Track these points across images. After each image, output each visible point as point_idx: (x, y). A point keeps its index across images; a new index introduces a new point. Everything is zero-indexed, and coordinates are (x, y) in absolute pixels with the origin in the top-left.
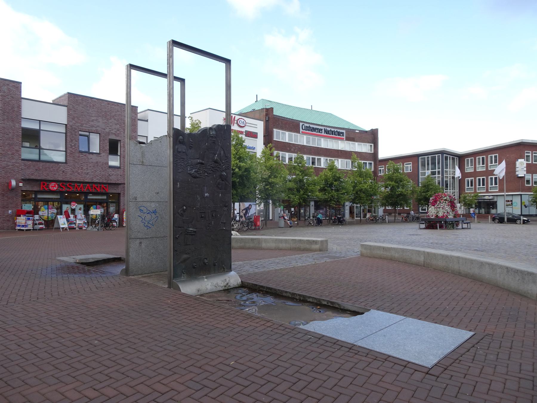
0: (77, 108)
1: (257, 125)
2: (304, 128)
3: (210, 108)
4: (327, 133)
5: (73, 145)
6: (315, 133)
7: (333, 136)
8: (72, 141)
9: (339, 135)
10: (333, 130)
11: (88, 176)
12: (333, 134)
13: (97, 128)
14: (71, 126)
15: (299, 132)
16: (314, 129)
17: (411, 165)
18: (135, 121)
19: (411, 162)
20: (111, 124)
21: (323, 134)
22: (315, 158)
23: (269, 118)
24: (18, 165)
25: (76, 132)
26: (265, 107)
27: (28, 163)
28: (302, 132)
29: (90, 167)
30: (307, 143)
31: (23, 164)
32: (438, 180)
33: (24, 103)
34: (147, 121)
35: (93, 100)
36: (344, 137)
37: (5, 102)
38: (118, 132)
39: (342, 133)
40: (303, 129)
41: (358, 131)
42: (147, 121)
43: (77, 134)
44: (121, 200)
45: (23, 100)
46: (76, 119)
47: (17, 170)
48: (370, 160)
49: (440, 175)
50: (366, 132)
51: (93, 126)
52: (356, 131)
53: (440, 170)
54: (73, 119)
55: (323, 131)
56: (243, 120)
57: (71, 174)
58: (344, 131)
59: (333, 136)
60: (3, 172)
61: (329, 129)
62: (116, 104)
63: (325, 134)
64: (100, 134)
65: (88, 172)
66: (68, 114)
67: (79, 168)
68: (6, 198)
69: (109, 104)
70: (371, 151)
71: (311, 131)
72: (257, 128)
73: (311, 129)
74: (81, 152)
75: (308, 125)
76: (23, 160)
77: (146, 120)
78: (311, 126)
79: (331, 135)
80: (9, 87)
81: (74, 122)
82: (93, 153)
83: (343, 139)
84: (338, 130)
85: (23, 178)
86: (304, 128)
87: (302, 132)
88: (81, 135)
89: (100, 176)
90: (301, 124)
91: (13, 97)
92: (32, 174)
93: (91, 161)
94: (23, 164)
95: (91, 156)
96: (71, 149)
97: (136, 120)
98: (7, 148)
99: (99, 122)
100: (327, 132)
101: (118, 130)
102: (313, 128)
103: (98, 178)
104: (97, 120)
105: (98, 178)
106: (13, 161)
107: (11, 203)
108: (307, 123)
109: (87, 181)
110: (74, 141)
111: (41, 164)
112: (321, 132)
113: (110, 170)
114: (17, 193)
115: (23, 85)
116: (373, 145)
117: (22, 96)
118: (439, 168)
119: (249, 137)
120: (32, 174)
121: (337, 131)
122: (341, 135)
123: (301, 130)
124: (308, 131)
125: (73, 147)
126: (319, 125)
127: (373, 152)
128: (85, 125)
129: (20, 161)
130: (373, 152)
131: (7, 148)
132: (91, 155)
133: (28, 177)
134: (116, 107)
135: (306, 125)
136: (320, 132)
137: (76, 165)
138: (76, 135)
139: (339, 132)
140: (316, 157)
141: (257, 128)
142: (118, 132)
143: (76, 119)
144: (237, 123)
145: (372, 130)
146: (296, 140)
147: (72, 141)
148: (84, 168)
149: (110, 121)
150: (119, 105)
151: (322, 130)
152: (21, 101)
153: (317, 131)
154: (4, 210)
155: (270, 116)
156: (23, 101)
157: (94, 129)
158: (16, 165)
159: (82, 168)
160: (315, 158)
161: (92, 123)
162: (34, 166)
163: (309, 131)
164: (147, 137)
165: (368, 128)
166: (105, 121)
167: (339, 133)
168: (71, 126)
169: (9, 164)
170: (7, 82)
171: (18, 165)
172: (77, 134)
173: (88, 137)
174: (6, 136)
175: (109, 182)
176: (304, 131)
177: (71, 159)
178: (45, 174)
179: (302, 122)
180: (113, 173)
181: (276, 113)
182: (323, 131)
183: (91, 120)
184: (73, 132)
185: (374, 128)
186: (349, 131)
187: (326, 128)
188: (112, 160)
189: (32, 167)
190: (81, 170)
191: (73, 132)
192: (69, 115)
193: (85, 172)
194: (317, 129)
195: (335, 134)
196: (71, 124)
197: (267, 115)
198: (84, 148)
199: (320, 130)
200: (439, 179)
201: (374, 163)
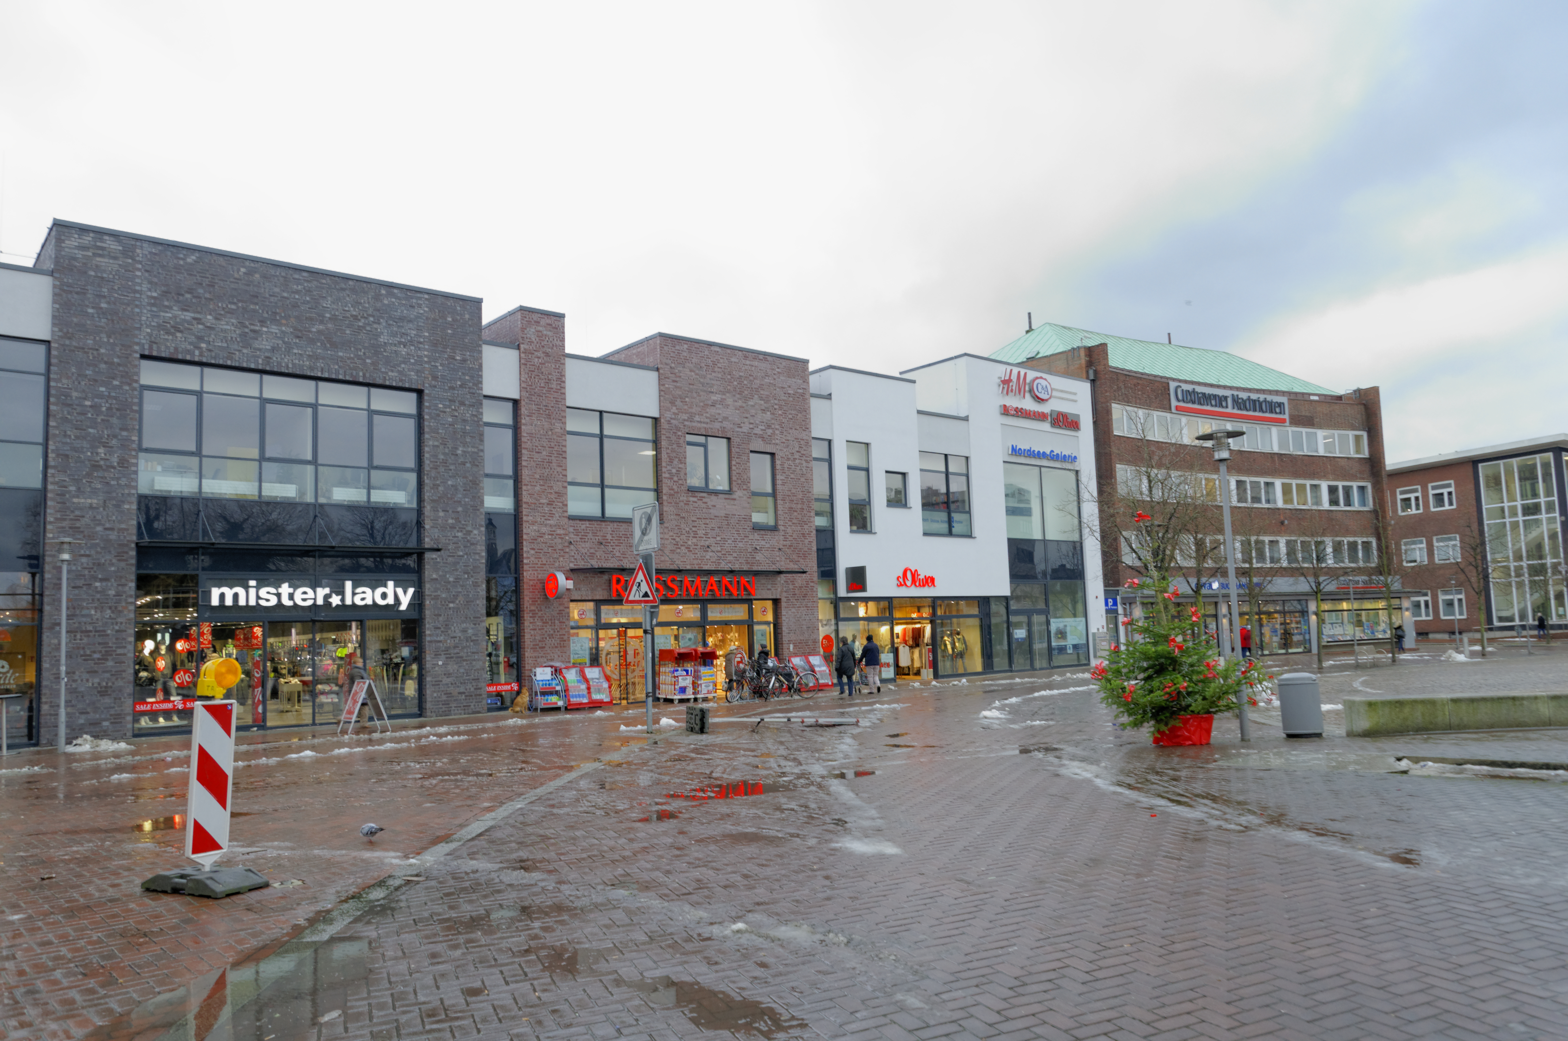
0: (680, 372)
1: (1075, 394)
2: (1180, 397)
3: (966, 354)
4: (1240, 409)
5: (674, 471)
6: (1209, 408)
7: (1257, 414)
8: (671, 461)
9: (1271, 412)
10: (1254, 396)
11: (711, 554)
12: (1255, 410)
13: (726, 424)
14: (669, 422)
15: (1169, 409)
16: (1206, 398)
17: (1452, 489)
18: (805, 400)
19: (1452, 482)
20: (753, 412)
21: (1229, 410)
22: (1291, 485)
23: (1096, 372)
24: (562, 532)
25: (679, 437)
26: (1080, 345)
27: (583, 527)
28: (1177, 408)
29: (713, 529)
30: (1280, 447)
31: (571, 529)
32: (1548, 530)
33: (570, 367)
34: (829, 397)
35: (713, 348)
36: (1286, 416)
37: (532, 368)
38: (769, 432)
39: (1280, 405)
40: (1178, 400)
41: (1316, 398)
42: (829, 397)
43: (681, 441)
44: (784, 618)
45: (568, 361)
46: (678, 403)
47: (560, 547)
48: (1363, 479)
49: (1557, 514)
50: (1340, 398)
51: (713, 420)
52: (1312, 398)
53: (1555, 498)
54: (673, 403)
55: (1230, 400)
56: (1044, 383)
57: (672, 551)
58: (1284, 399)
59: (1257, 414)
60: (532, 552)
61: (1243, 395)
62: (761, 357)
63: (1236, 411)
64: (729, 439)
65: (707, 543)
66: (660, 391)
67: (688, 532)
68: (539, 623)
69: (746, 357)
70: (1358, 451)
71: (1200, 404)
72: (1075, 401)
73: (1199, 399)
74: (692, 490)
75: (1189, 387)
76: (572, 518)
77: (826, 393)
78: (1199, 389)
79: (1251, 413)
80: (540, 328)
81: (674, 410)
82: (716, 493)
83: (1284, 421)
84: (1269, 398)
85: (572, 566)
86: (1180, 397)
87: (1177, 408)
88: (690, 444)
89: (735, 555)
90: (1173, 385)
91: (547, 355)
92: (592, 555)
93: (713, 512)
94: (571, 529)
95: (712, 500)
96: (670, 483)
97: (807, 396)
98: (538, 488)
99: (727, 406)
100: (1238, 403)
101: (769, 427)
102: (1204, 394)
103: (730, 558)
104: (723, 400)
105: (730, 558)
106: (551, 522)
107: (551, 636)
108: (1186, 382)
109: (706, 568)
110: (676, 462)
111: (610, 527)
112: (1224, 404)
113: (756, 536)
114: (561, 608)
115: (568, 322)
116: (1365, 434)
117: (568, 350)
118: (1549, 493)
119: (1060, 427)
120: (592, 555)
121: (1265, 400)
122: (1278, 410)
123: (1174, 403)
124: (1190, 405)
125: (675, 479)
126: (1211, 385)
127: (1366, 454)
128: (697, 418)
129: (566, 520)
130: (1366, 454)
131: (538, 488)
132: (713, 497)
133: (582, 565)
134: (763, 365)
135: (1186, 387)
136: (1221, 406)
137: (682, 526)
138: (679, 446)
139: (1271, 403)
140: (1262, 480)
141: (1075, 401)
142: (769, 432)
143: (678, 403)
144: (1031, 391)
145: (1358, 391)
146: (1298, 437)
147: (671, 461)
148: (701, 533)
149: (751, 403)
150: (769, 358)
151: (1226, 398)
152: (564, 364)
153: (1213, 402)
154: (536, 654)
155: (1100, 368)
156: (568, 361)
157: (717, 425)
158: (559, 532)
159: (695, 533)
160: (1305, 485)
161: (712, 411)
162: (595, 534)
163: (1194, 403)
164: (830, 441)
165: (1343, 386)
166: (740, 403)
167: (1273, 407)
168: (669, 422)
169: (544, 529)
170: (535, 317)
171: (562, 532)
172: (681, 441)
173: (705, 446)
174: (536, 456)
175: (755, 568)
176: (1182, 404)
177: (672, 509)
178: (618, 554)
179: (1174, 380)
180: (763, 543)
181: (1117, 359)
182: (1230, 400)
183: (710, 403)
184: (674, 438)
185: (1364, 386)
186: (1298, 399)
187: (1235, 393)
188: (494, 494)
189: (590, 535)
190: (695, 540)
191: (674, 438)
192: (663, 392)
193: (702, 543)
194: (1215, 396)
195: (1261, 410)
196: (668, 415)
197: (1090, 364)
198: (696, 481)
199: (1221, 401)
200: (1552, 526)
201: (1374, 486)
